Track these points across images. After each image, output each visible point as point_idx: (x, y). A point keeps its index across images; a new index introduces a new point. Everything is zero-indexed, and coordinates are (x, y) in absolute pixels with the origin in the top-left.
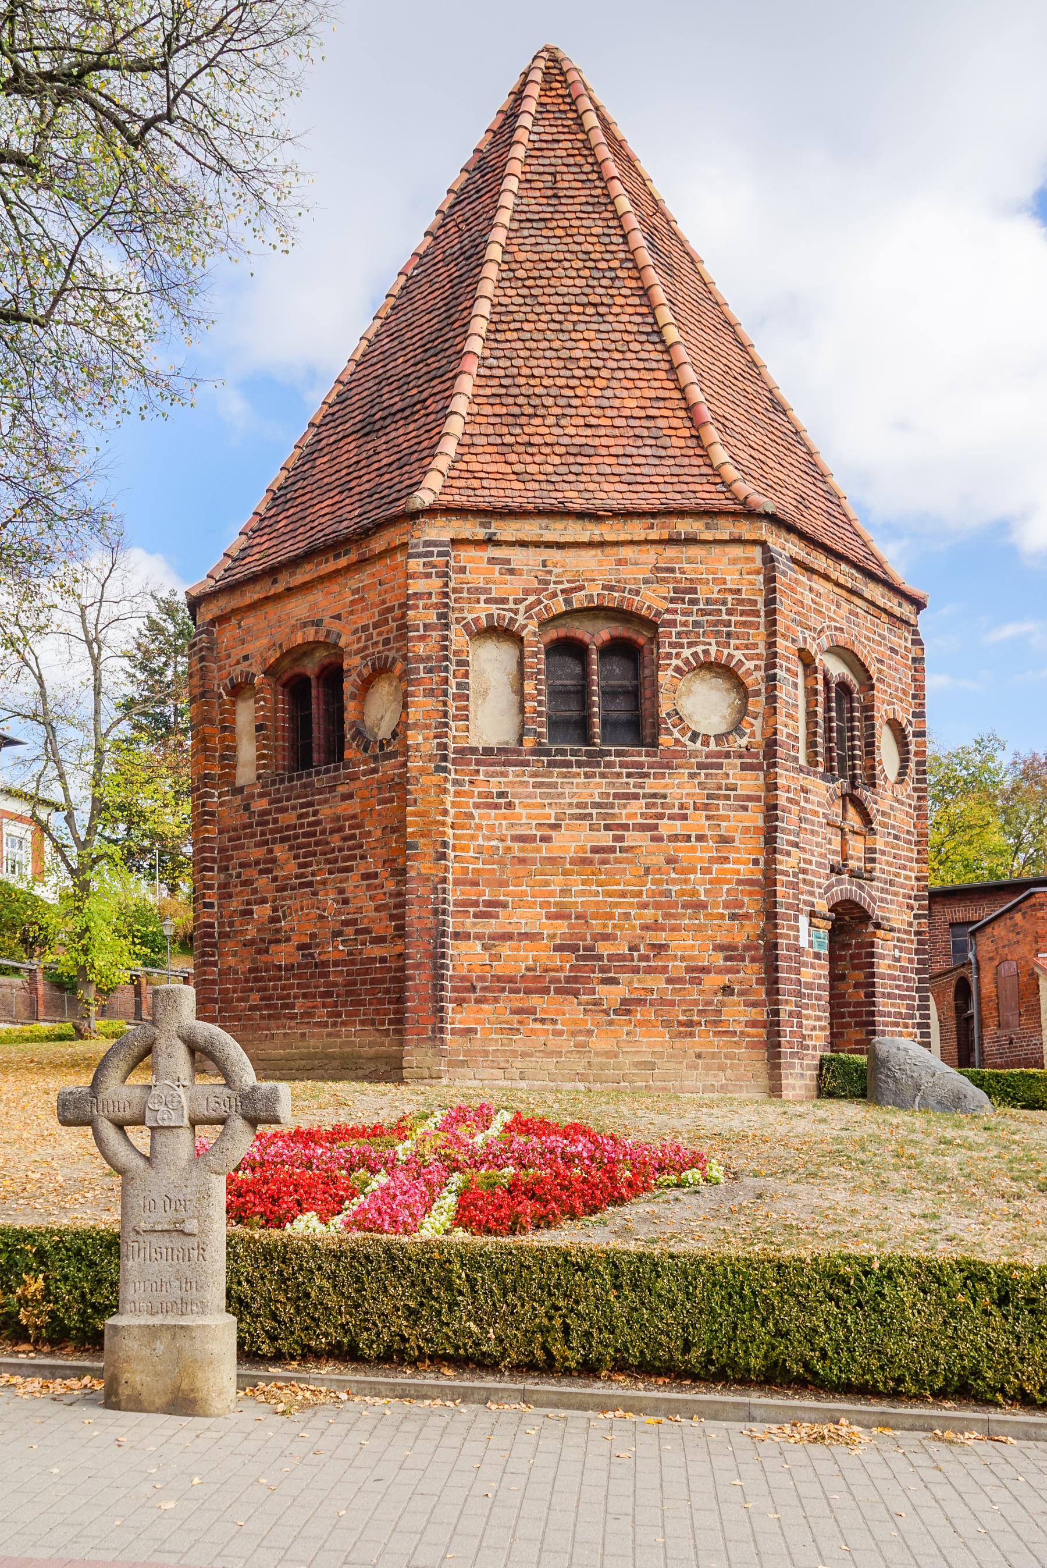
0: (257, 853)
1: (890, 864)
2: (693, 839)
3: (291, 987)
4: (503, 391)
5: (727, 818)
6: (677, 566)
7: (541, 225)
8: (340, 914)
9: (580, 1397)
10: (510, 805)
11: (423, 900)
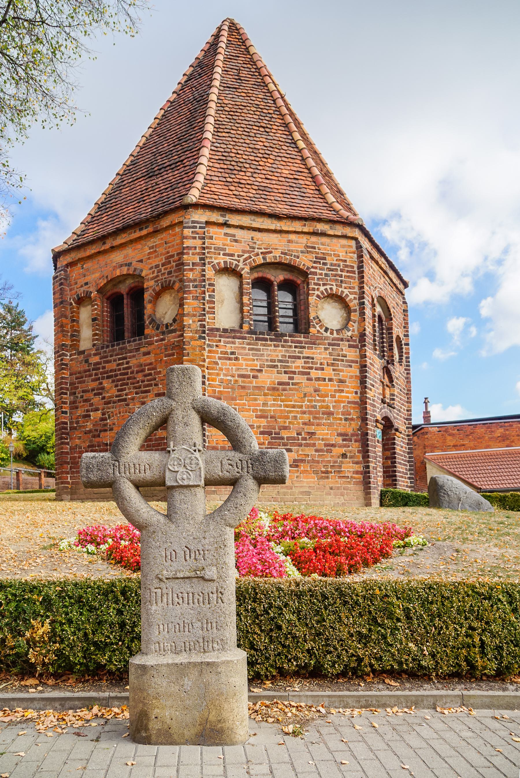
1: (399, 402)
2: (327, 380)
4: (224, 158)
5: (342, 371)
6: (316, 246)
7: (234, 90)
9: (507, 699)
10: (237, 359)
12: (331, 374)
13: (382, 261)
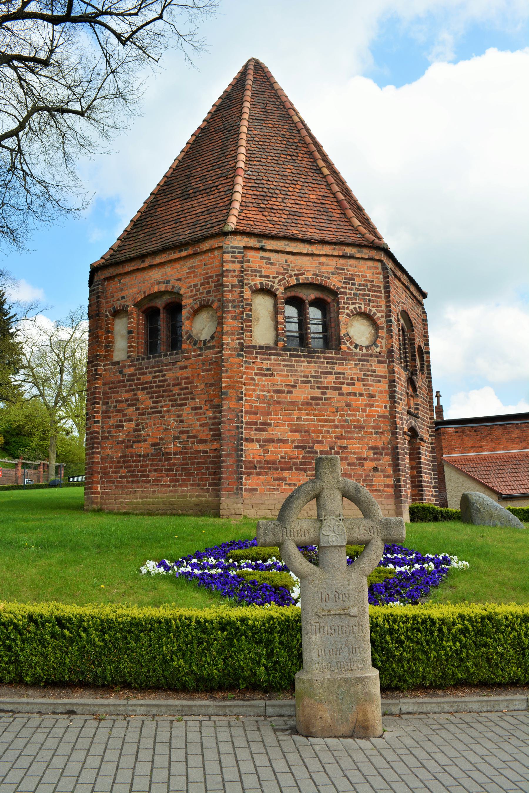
0: (126, 395)
1: (422, 411)
3: (147, 466)
4: (257, 185)
7: (262, 122)
8: (178, 427)
10: (272, 375)
11: (231, 421)
12: (361, 389)
13: (404, 278)
